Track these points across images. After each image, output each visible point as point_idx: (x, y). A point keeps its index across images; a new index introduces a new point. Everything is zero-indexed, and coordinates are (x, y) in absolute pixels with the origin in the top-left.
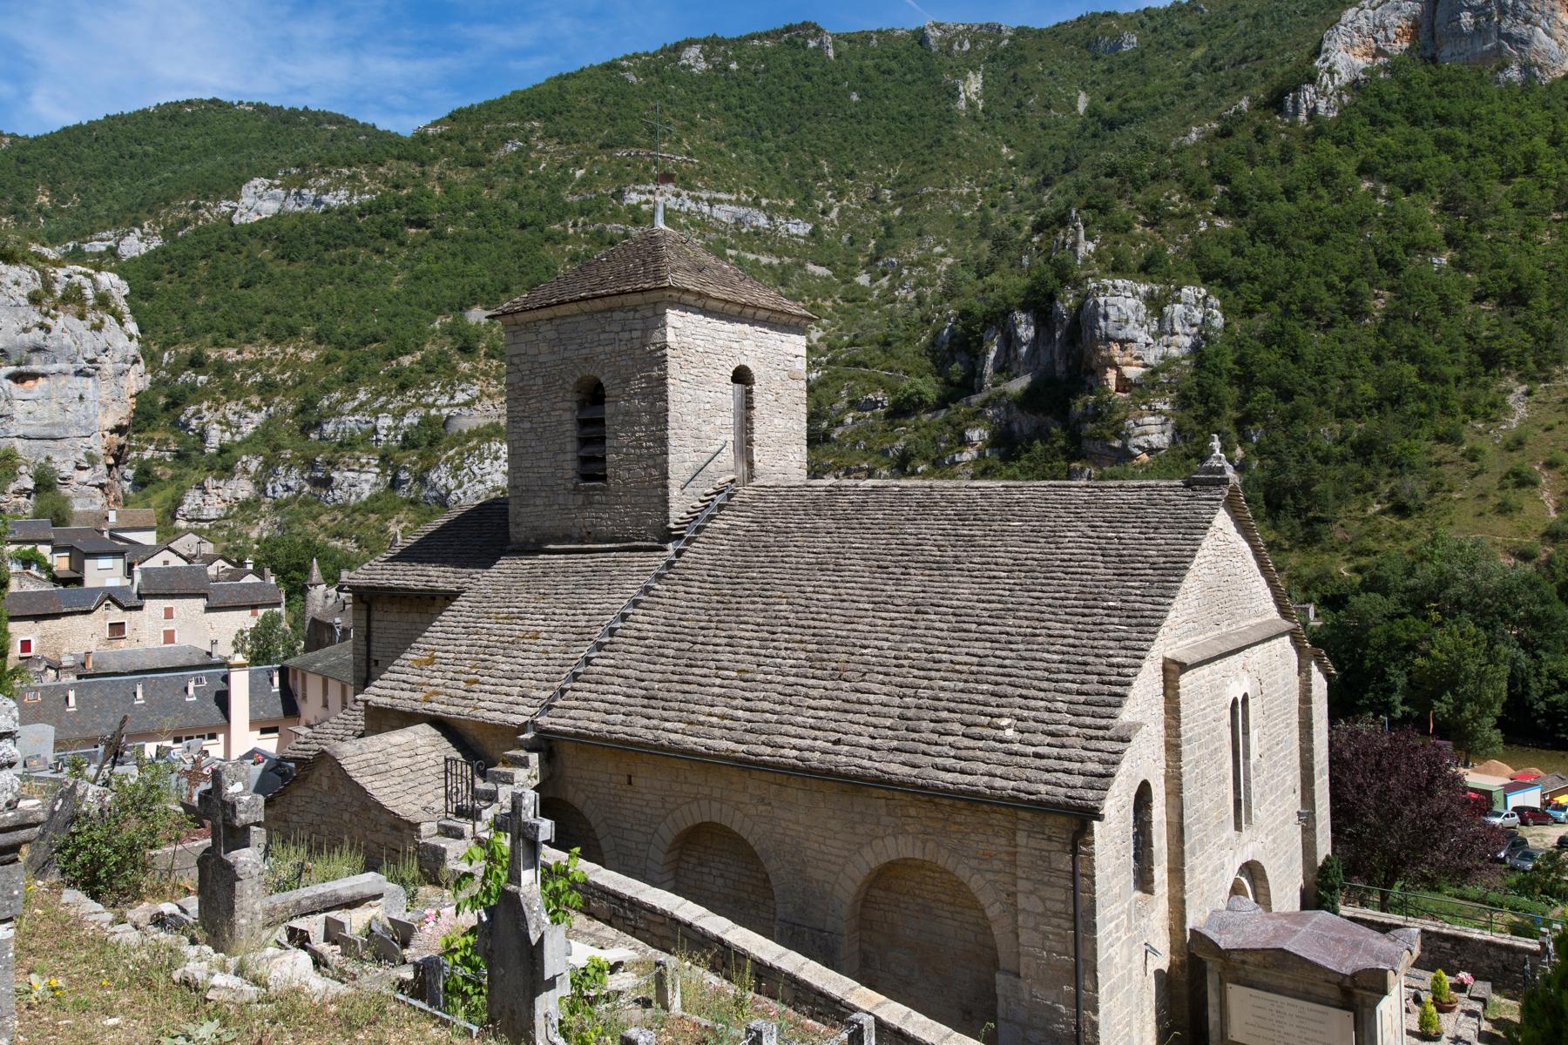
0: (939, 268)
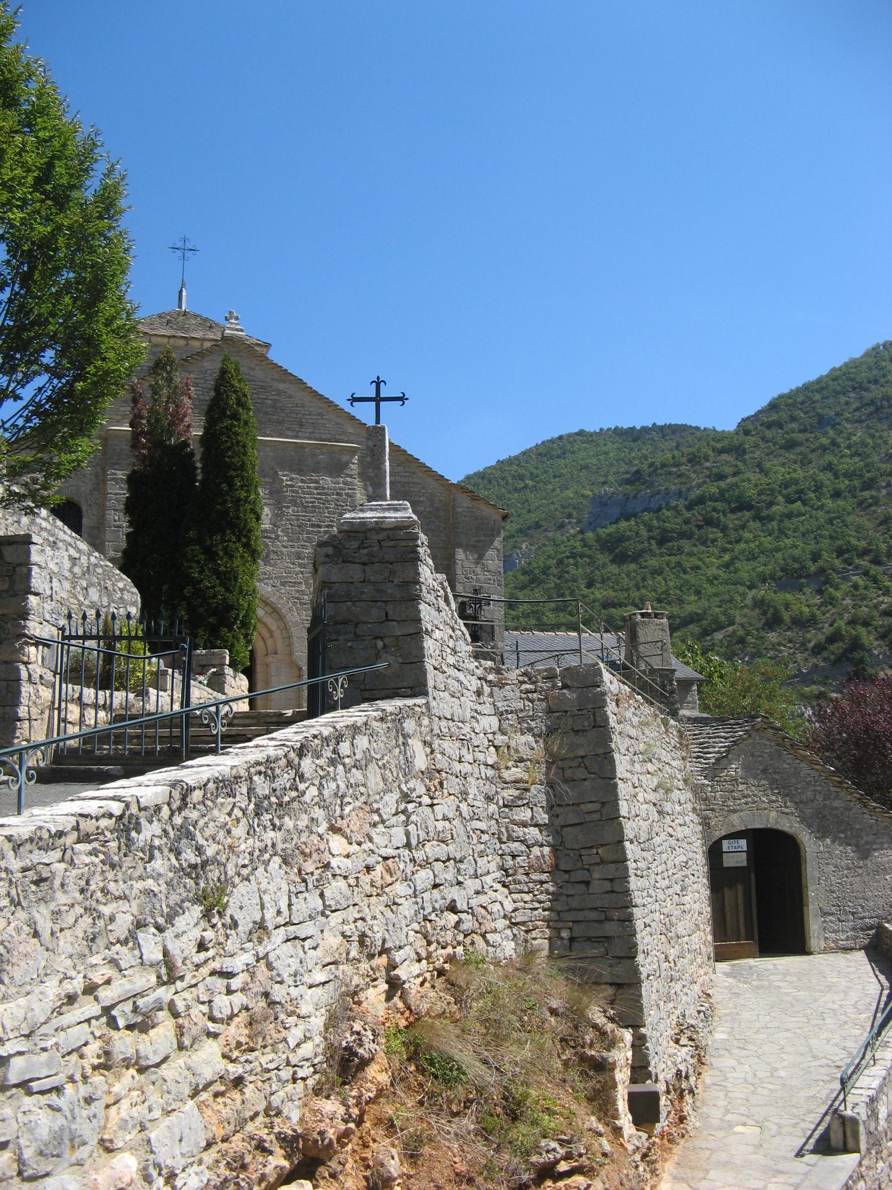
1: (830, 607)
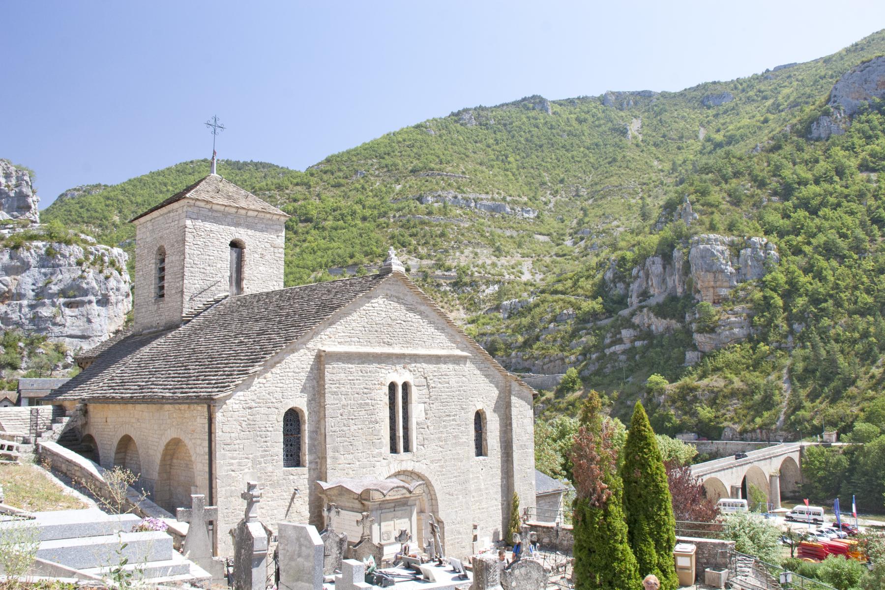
0: (615, 234)
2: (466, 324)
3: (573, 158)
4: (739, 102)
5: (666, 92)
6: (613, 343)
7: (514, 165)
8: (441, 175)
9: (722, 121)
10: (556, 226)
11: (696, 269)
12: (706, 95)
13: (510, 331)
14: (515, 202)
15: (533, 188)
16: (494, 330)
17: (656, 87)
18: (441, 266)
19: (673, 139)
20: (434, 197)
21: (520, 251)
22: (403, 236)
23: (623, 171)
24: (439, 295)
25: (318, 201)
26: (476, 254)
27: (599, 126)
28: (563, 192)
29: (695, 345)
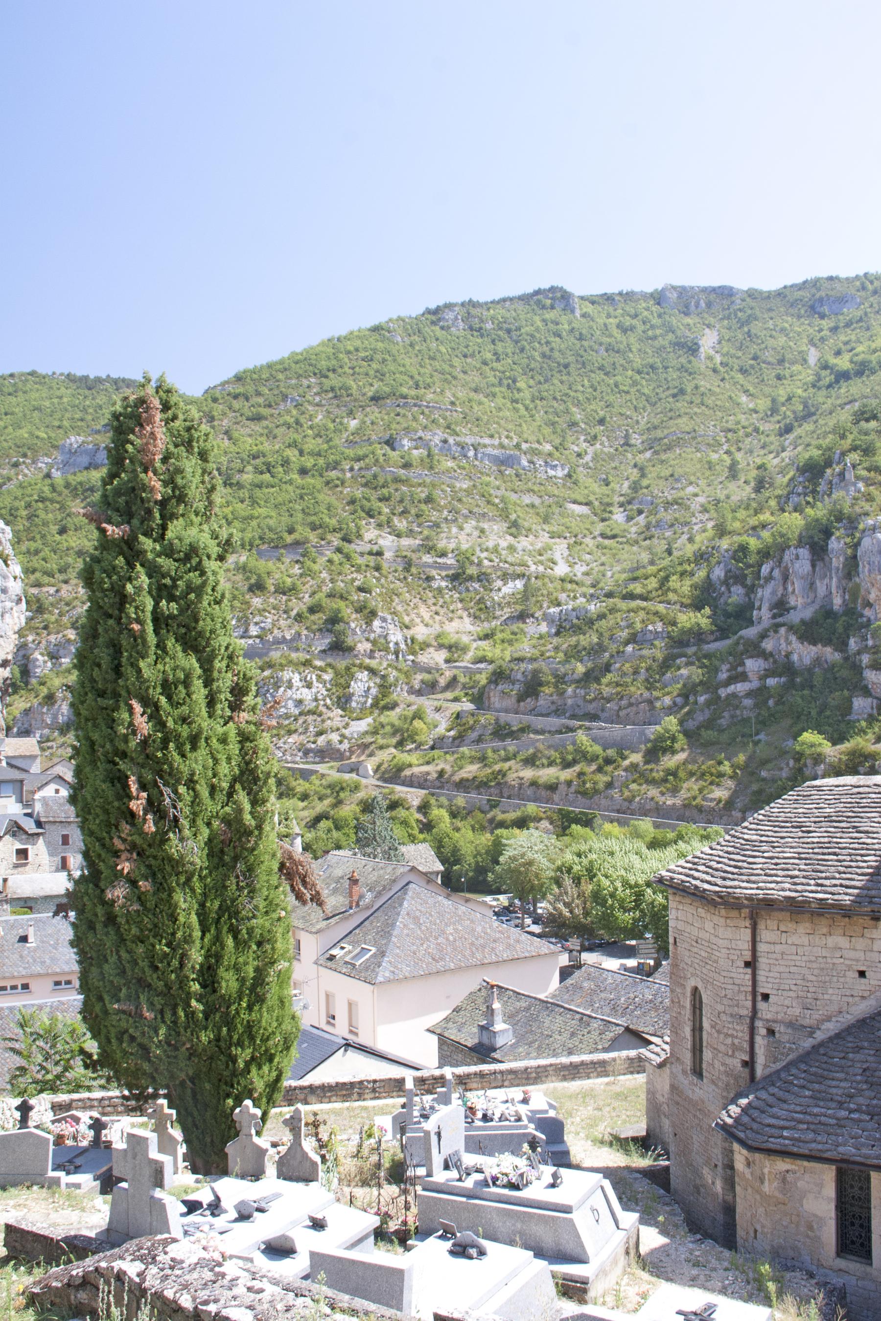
0: (693, 506)
1: (309, 578)
2: (475, 640)
3: (616, 386)
4: (869, 310)
5: (756, 290)
6: (731, 680)
7: (527, 395)
8: (420, 406)
9: (843, 338)
10: (597, 490)
11: (870, 571)
12: (817, 296)
13: (561, 655)
14: (534, 452)
15: (559, 430)
16: (536, 652)
17: (741, 283)
18: (431, 549)
19: (769, 363)
20: (412, 440)
21: (546, 527)
22: (369, 500)
23: (696, 409)
24: (430, 595)
25: (226, 442)
26: (482, 531)
27: (654, 338)
28: (604, 439)
29: (866, 687)
